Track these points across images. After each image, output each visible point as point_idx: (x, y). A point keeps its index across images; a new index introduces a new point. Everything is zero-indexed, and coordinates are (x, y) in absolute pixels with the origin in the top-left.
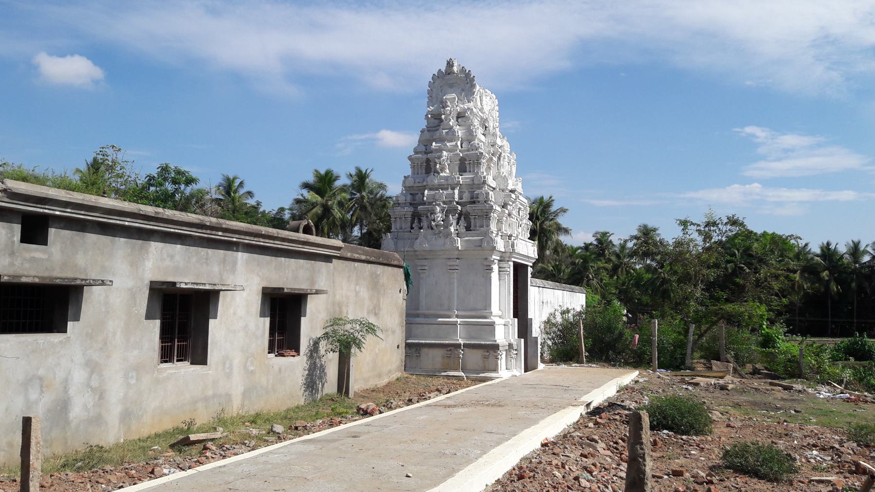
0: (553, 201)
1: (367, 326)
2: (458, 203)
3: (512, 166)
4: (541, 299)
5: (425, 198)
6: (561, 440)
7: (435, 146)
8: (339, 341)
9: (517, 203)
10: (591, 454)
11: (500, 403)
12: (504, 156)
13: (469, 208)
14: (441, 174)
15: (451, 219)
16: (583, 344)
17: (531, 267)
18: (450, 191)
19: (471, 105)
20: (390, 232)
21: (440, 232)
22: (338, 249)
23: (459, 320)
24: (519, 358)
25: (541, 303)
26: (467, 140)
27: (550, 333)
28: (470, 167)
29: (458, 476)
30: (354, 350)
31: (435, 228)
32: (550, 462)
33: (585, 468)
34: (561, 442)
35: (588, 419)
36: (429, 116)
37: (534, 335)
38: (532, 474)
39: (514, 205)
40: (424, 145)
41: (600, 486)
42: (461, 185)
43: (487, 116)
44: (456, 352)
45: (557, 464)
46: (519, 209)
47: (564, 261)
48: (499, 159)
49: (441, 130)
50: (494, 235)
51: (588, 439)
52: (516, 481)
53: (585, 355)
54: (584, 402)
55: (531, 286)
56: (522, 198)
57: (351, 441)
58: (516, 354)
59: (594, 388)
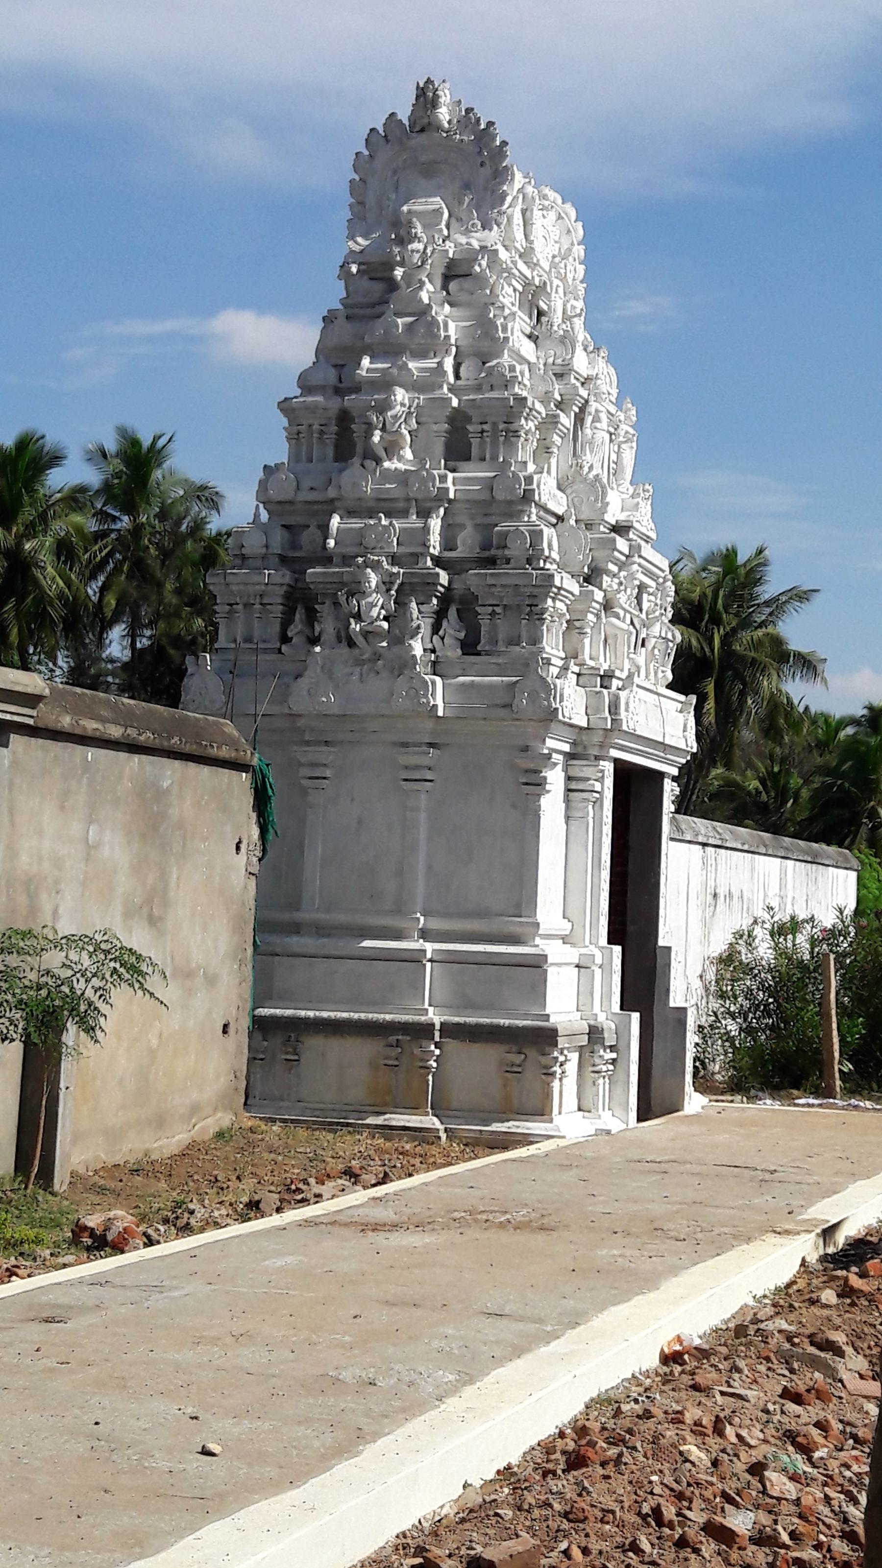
0: (765, 564)
1: (115, 960)
2: (438, 561)
3: (623, 446)
4: (711, 883)
5: (331, 543)
6: (725, 1345)
7: (368, 371)
8: (20, 1004)
9: (635, 567)
10: (817, 1391)
11: (545, 1221)
12: (597, 411)
13: (474, 578)
14: (386, 464)
15: (415, 613)
16: (835, 1033)
17: (674, 779)
18: (413, 521)
19: (492, 237)
20: (213, 651)
21: (377, 656)
22: (30, 700)
23: (429, 947)
24: (620, 1075)
25: (710, 898)
26: (476, 355)
27: (735, 997)
28: (482, 445)
29: (371, 1451)
30: (71, 1034)
31: (360, 640)
32: (678, 1412)
33: (791, 1437)
34: (724, 1350)
35: (825, 1278)
36: (354, 269)
37: (676, 1000)
38: (613, 1452)
39: (623, 574)
40: (335, 366)
41: (832, 1494)
42: (450, 501)
43: (545, 277)
44: (417, 1051)
45: (700, 1420)
46: (639, 587)
47: (801, 762)
48: (579, 419)
49: (389, 317)
50: (554, 671)
51: (812, 1344)
52: (559, 1472)
53: (840, 1071)
54: (814, 1222)
55: (672, 839)
56: (652, 551)
57: (36, 1332)
58: (614, 1062)
59: (854, 1177)
